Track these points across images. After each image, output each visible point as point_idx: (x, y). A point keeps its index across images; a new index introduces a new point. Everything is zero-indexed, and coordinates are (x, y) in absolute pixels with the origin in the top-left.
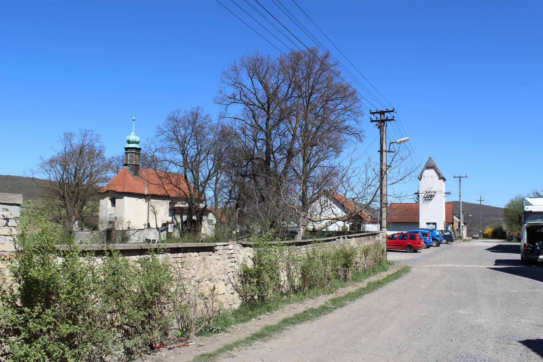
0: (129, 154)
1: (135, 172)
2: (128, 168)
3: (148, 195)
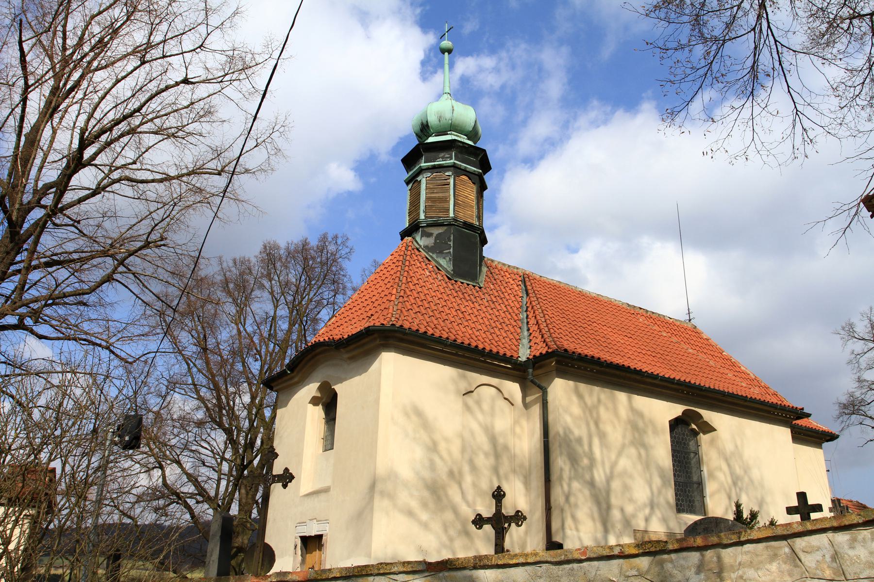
0: (423, 179)
1: (457, 261)
2: (422, 241)
3: (537, 361)
